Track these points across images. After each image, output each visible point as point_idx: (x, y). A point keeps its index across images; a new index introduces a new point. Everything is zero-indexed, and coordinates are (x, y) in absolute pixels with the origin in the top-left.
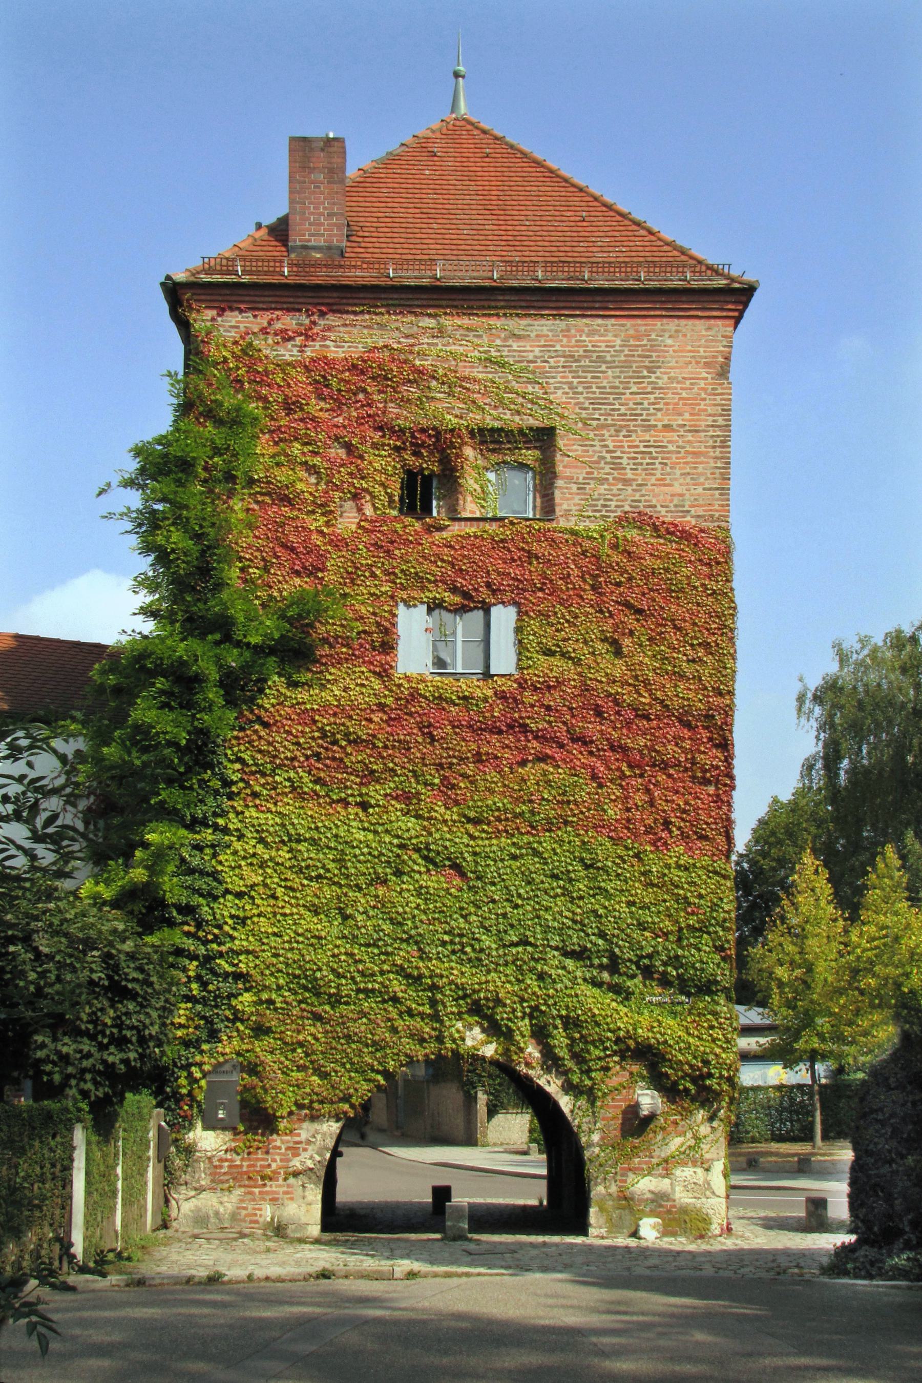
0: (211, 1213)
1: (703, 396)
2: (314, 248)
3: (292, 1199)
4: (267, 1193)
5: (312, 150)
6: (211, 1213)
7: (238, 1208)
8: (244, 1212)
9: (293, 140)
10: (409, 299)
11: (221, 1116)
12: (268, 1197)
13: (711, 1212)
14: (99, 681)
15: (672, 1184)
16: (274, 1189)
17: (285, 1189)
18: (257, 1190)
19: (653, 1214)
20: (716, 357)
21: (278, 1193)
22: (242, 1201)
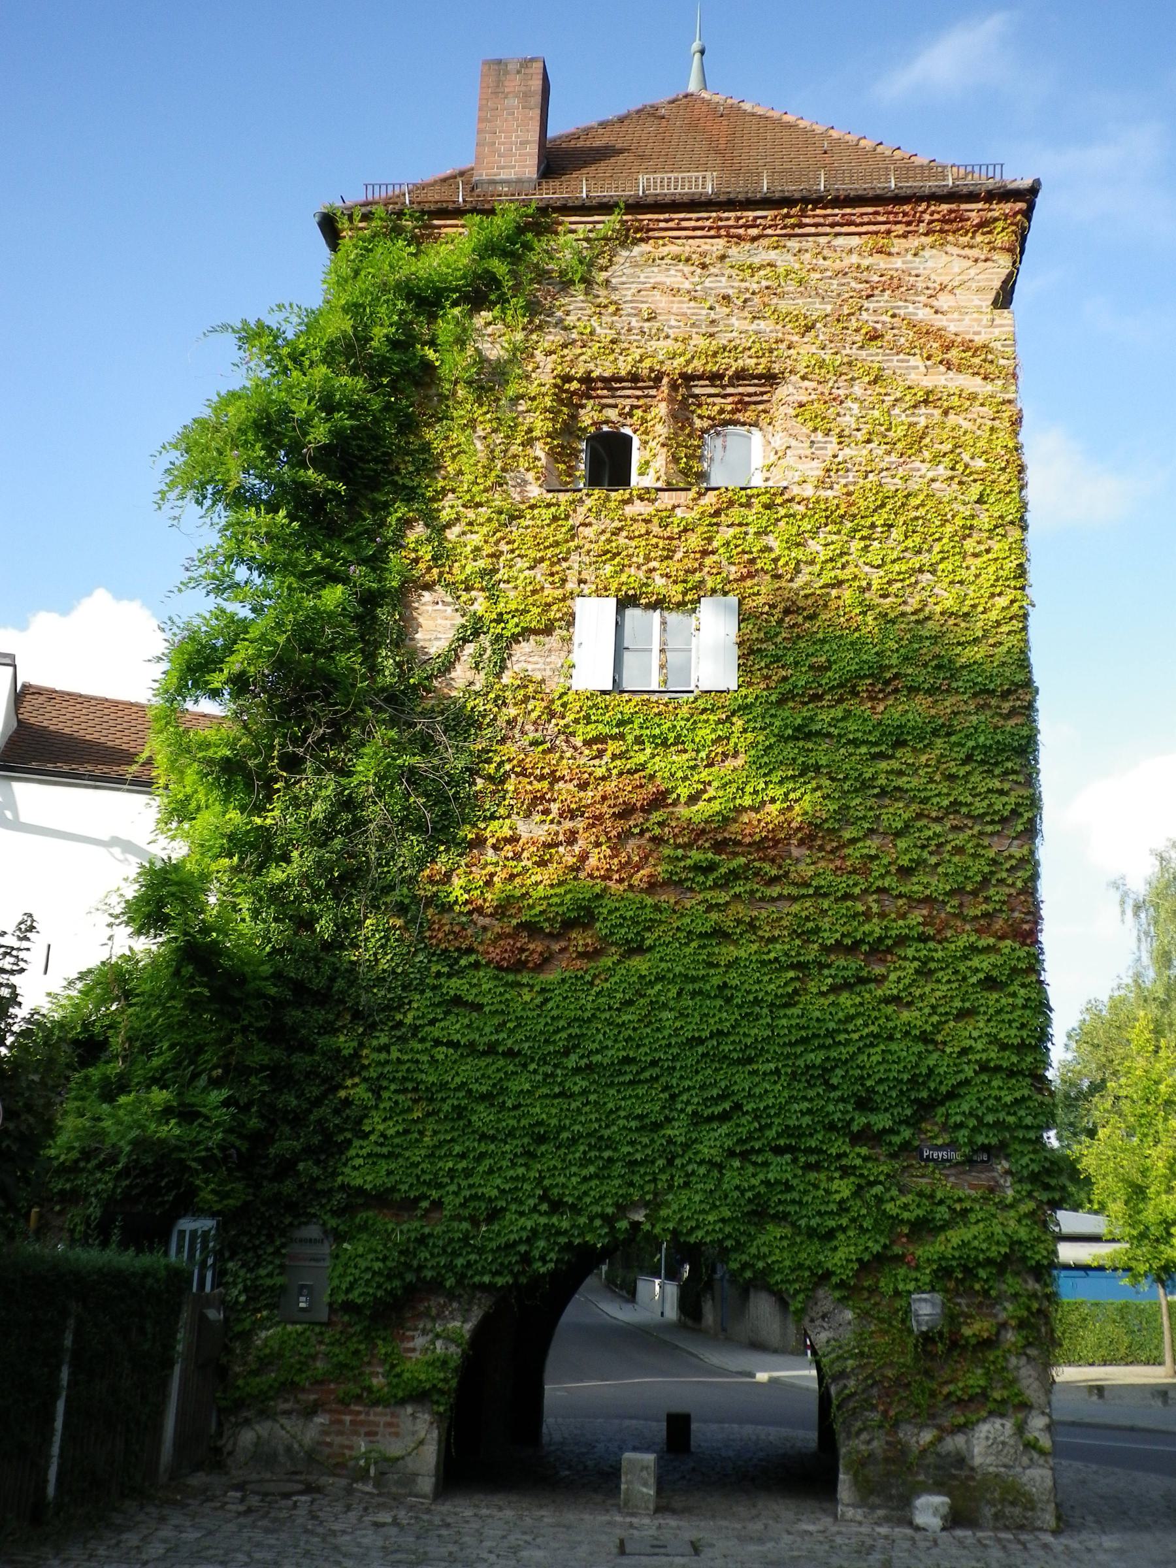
0: (281, 1449)
1: (977, 329)
2: (502, 182)
3: (397, 1435)
4: (362, 1423)
5: (507, 73)
6: (281, 1449)
7: (319, 1443)
8: (327, 1450)
9: (486, 63)
10: (698, 219)
11: (302, 1305)
12: (363, 1430)
13: (754, 1512)
14: (707, 650)
15: (967, 1442)
16: (372, 1418)
17: (388, 1419)
18: (348, 1418)
19: (939, 1487)
20: (992, 280)
21: (377, 1424)
22: (325, 1433)
